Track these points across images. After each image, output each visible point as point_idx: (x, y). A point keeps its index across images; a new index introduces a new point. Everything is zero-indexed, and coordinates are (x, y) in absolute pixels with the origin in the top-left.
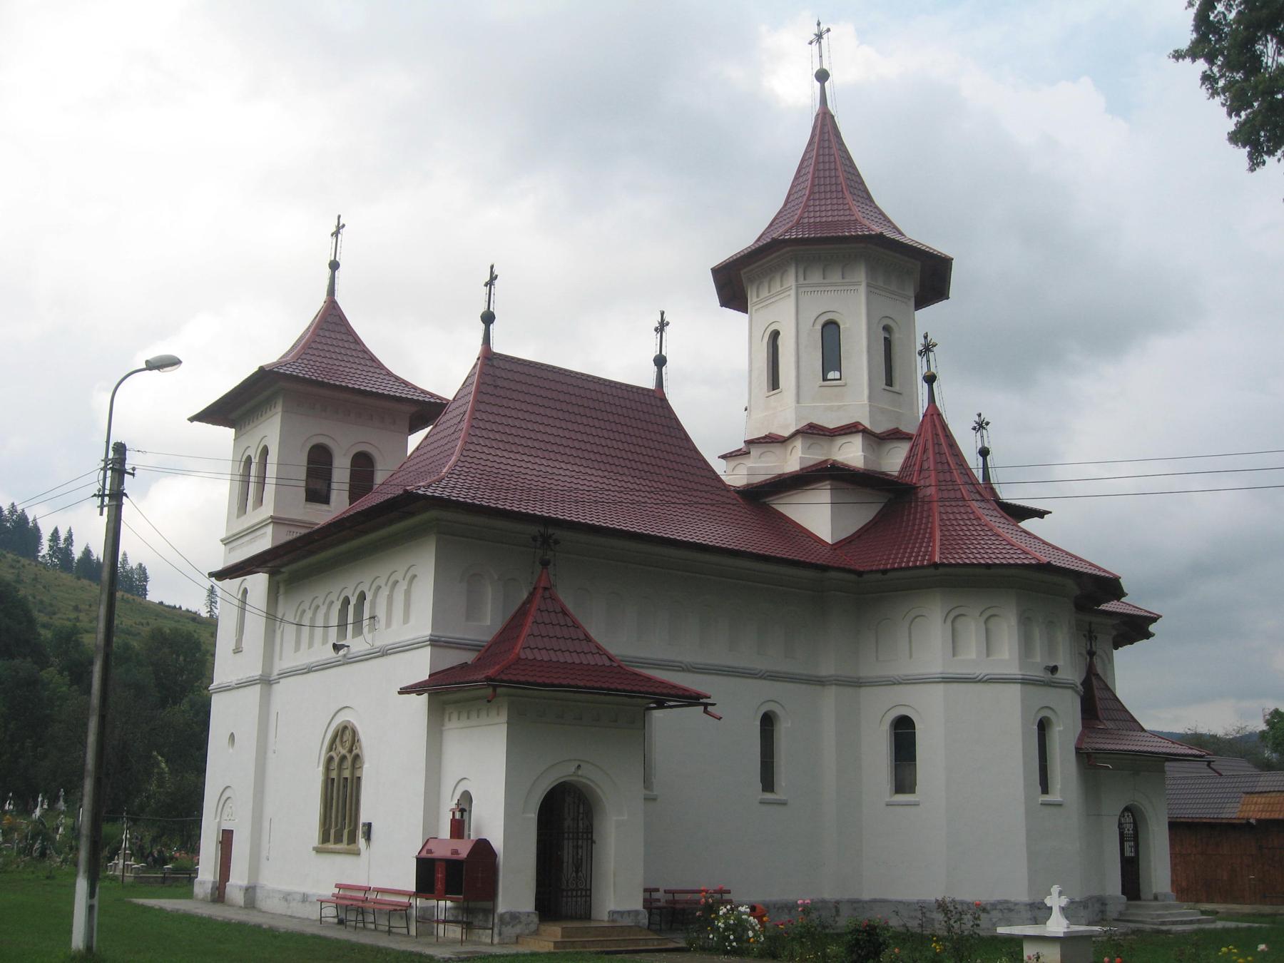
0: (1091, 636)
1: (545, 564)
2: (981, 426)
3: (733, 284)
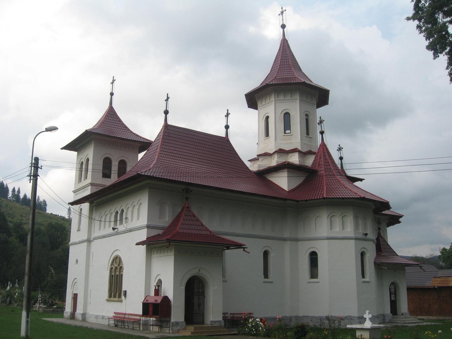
0: (379, 223)
1: (187, 199)
2: (340, 149)
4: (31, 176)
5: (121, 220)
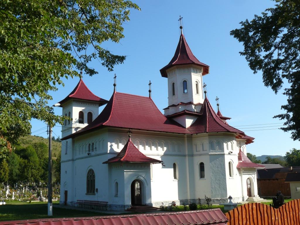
3: (164, 72)
4: (48, 131)
5: (93, 150)
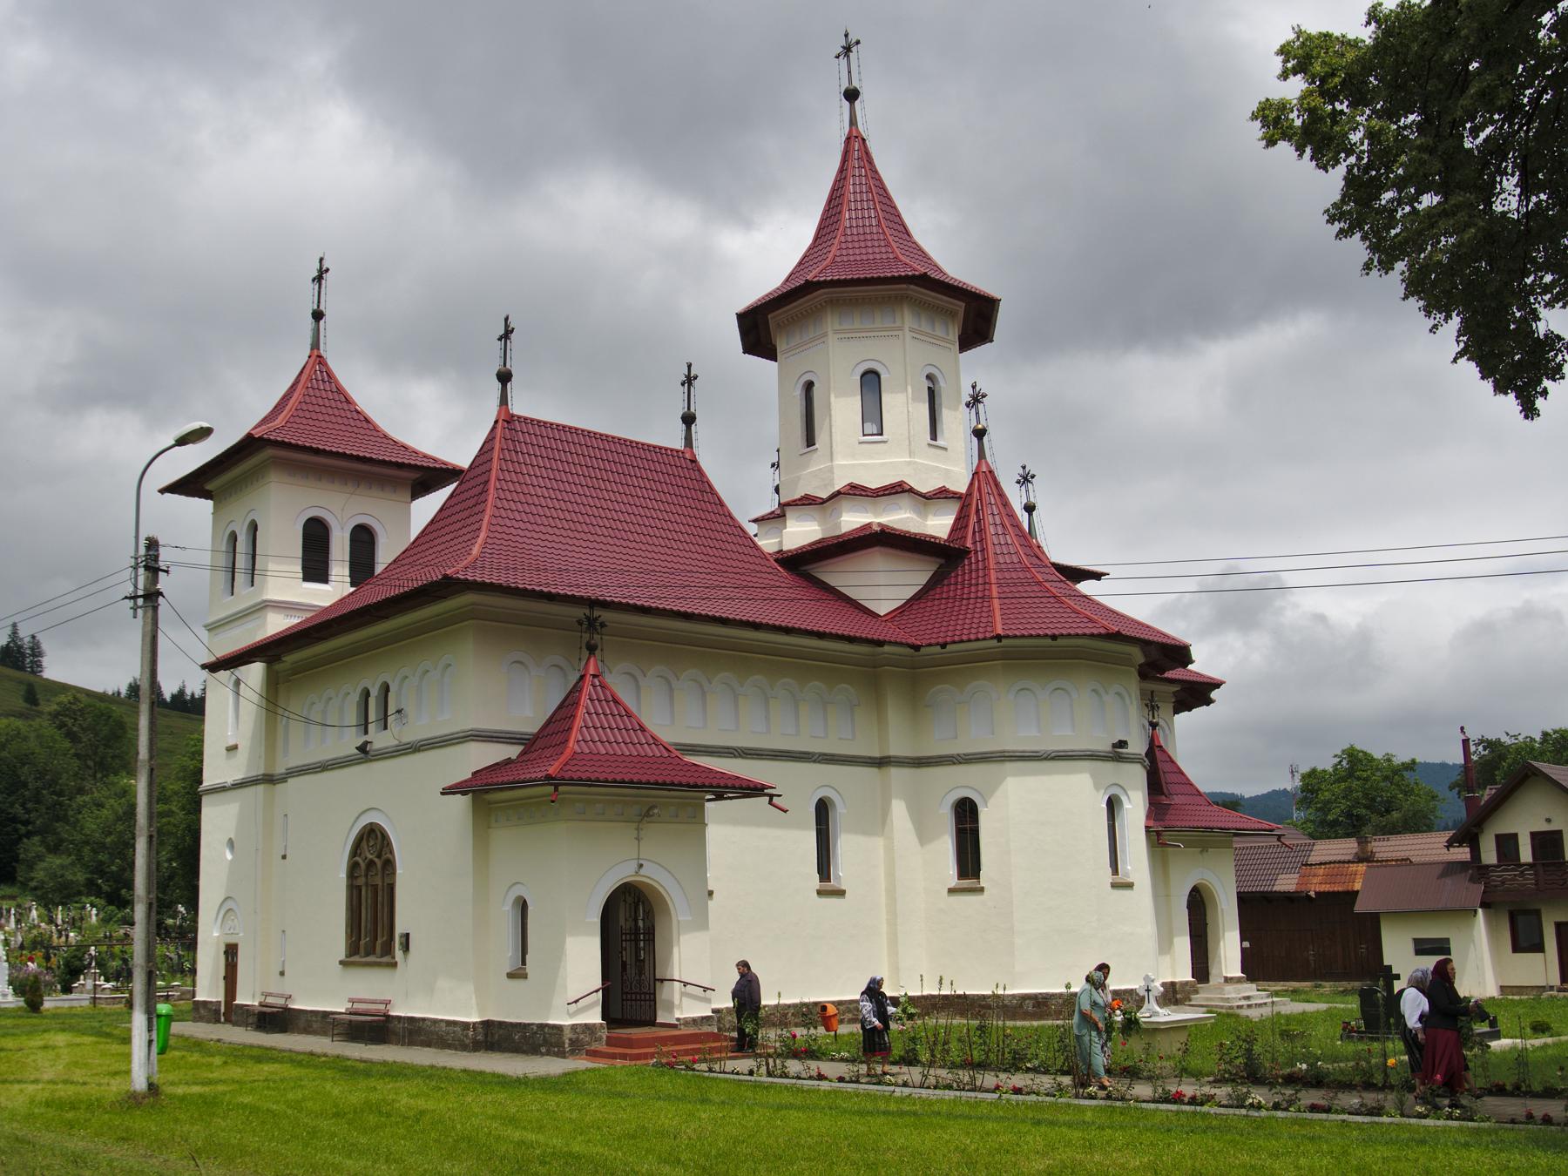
0: (1152, 707)
1: (592, 649)
2: (1026, 479)
